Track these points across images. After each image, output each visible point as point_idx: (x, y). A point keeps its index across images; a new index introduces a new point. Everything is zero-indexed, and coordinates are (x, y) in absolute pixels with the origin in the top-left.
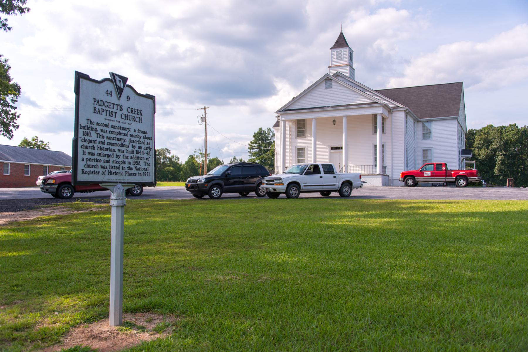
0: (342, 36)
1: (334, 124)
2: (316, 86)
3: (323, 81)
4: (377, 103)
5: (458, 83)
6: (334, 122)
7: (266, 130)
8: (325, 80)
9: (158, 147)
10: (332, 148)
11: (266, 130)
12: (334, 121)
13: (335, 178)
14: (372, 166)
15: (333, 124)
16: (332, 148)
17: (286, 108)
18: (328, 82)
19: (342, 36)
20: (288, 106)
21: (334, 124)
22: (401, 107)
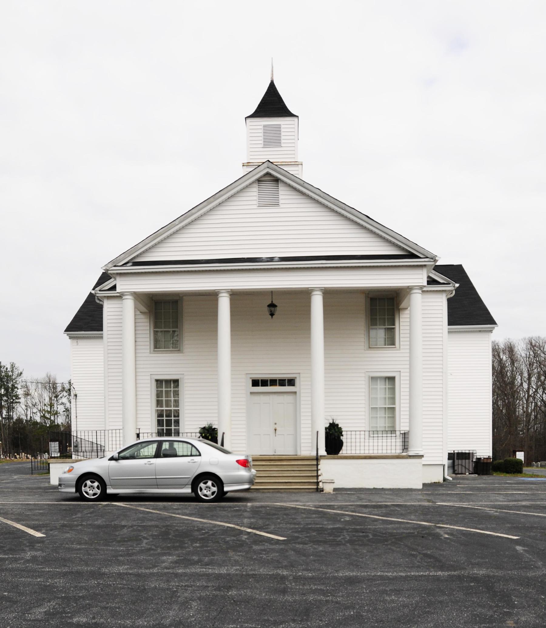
0: (272, 91)
1: (272, 315)
2: (232, 196)
3: (253, 183)
4: (412, 256)
5: (453, 265)
6: (273, 309)
7: (9, 367)
8: (259, 181)
9: (420, 487)
10: (255, 383)
11: (9, 367)
12: (272, 306)
13: (136, 436)
14: (367, 433)
15: (268, 313)
16: (255, 383)
17: (138, 256)
18: (268, 187)
19: (272, 91)
20: (144, 252)
21: (272, 315)
22: (442, 281)
